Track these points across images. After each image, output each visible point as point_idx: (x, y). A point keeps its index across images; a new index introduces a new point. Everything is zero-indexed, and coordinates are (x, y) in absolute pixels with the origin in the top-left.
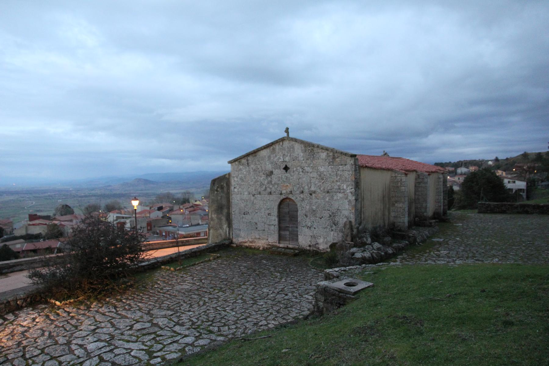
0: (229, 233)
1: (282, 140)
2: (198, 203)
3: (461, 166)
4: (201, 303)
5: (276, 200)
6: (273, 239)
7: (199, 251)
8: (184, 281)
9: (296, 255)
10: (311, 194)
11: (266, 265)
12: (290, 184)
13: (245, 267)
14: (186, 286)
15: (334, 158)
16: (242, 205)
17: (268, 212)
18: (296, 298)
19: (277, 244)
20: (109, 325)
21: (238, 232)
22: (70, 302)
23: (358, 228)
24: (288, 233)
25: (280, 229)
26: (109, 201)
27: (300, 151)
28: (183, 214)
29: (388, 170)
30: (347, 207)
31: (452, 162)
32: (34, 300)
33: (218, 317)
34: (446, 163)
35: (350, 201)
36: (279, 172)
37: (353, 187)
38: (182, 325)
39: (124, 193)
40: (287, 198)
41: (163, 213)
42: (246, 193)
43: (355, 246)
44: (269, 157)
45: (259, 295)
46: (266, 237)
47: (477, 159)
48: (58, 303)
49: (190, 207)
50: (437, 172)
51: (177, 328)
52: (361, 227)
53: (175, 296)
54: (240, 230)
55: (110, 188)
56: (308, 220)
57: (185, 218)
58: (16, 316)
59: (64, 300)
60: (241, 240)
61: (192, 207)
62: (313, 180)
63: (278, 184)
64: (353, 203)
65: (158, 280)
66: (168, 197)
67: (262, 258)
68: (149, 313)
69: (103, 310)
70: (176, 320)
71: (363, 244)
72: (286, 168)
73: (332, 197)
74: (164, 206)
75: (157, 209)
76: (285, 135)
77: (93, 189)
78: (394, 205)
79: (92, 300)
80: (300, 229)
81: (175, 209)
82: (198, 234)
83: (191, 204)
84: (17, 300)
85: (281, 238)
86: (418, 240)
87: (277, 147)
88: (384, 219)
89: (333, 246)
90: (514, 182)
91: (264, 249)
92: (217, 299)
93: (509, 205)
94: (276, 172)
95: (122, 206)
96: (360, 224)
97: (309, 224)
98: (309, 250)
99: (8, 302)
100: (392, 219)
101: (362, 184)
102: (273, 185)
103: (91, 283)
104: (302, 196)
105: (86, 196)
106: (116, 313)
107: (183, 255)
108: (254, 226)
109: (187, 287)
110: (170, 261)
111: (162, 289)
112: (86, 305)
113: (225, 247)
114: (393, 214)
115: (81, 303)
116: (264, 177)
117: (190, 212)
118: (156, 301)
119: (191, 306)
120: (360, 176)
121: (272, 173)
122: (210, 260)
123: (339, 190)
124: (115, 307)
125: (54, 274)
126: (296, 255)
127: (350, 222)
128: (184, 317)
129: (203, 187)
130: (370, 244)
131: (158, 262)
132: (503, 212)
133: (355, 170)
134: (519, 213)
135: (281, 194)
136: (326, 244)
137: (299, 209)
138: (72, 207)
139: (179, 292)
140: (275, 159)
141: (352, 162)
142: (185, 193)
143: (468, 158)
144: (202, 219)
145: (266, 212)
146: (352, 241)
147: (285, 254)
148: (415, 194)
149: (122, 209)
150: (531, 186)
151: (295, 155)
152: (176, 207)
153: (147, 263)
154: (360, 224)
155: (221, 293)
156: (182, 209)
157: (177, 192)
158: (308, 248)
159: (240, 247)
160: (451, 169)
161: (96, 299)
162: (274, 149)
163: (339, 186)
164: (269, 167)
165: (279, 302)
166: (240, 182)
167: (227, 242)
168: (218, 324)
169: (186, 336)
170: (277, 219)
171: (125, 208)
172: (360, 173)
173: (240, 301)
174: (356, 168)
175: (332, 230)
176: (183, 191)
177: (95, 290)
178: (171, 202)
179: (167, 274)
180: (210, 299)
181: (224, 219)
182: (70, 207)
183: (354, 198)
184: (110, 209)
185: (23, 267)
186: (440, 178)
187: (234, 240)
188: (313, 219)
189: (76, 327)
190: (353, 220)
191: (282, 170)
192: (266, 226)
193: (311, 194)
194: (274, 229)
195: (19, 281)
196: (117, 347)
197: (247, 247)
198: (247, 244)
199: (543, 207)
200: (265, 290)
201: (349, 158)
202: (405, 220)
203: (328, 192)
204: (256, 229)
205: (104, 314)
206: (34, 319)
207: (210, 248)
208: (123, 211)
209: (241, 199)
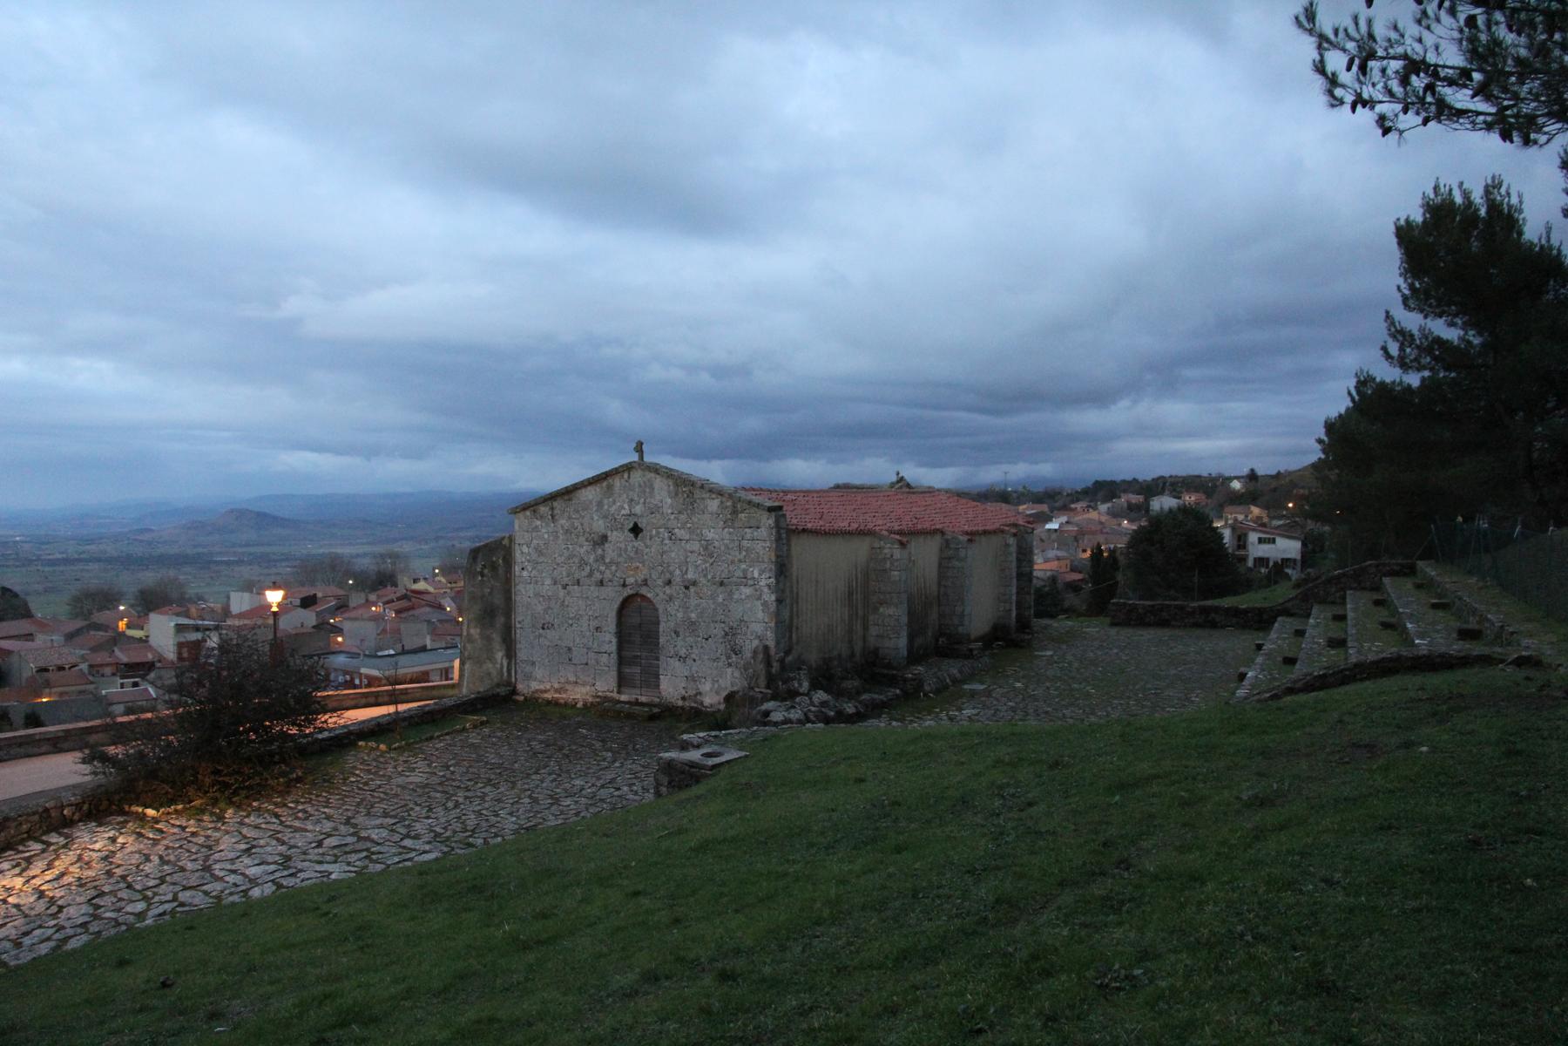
0: (509, 671)
1: (629, 468)
2: (421, 586)
3: (1162, 493)
4: (450, 805)
5: (612, 597)
6: (606, 685)
7: (439, 711)
8: (413, 770)
9: (652, 718)
10: (687, 588)
11: (585, 737)
12: (643, 562)
13: (541, 742)
14: (416, 778)
15: (735, 512)
16: (540, 608)
17: (594, 624)
18: (636, 793)
19: (615, 695)
20: (274, 842)
21: (528, 668)
22: (176, 811)
23: (782, 661)
24: (637, 670)
25: (621, 661)
26: (149, 578)
27: (664, 493)
28: (377, 618)
29: (862, 533)
30: (760, 615)
31: (1141, 478)
32: (98, 807)
33: (484, 824)
34: (1124, 481)
35: (765, 604)
36: (619, 538)
37: (772, 574)
38: (417, 837)
39: (189, 551)
40: (637, 595)
41: (318, 614)
42: (548, 581)
43: (774, 698)
44: (600, 504)
45: (566, 790)
46: (589, 679)
47: (1205, 474)
48: (151, 812)
49: (399, 599)
50: (1003, 531)
51: (408, 843)
52: (790, 658)
53: (396, 795)
54: (533, 663)
55: (147, 537)
56: (680, 643)
57: (384, 631)
58: (70, 840)
59: (162, 806)
60: (535, 686)
61: (404, 597)
62: (692, 558)
63: (617, 564)
64: (773, 608)
65: (355, 768)
66: (335, 568)
67: (580, 725)
68: (348, 822)
69: (252, 820)
70: (403, 831)
71: (793, 694)
72: (636, 530)
73: (731, 593)
74: (320, 595)
75: (298, 602)
76: (635, 457)
77: (91, 541)
78: (876, 610)
79: (222, 805)
80: (662, 663)
81: (352, 605)
82: (424, 677)
83: (401, 591)
84: (62, 807)
85: (623, 682)
86: (927, 688)
87: (617, 482)
88: (850, 641)
89: (729, 698)
90: (1274, 541)
91: (585, 705)
92: (483, 798)
93: (1176, 607)
94: (614, 536)
95: (191, 591)
96: (788, 652)
97: (683, 652)
98: (682, 708)
99: (47, 810)
100: (872, 642)
101: (795, 568)
102: (608, 566)
103: (217, 772)
104: (668, 590)
105: (67, 561)
106: (282, 823)
107: (405, 719)
108: (565, 655)
109: (418, 780)
110: (375, 731)
111: (366, 784)
112: (212, 814)
113: (498, 702)
114: (873, 631)
115: (202, 811)
116: (587, 547)
117: (398, 612)
118: (359, 804)
119: (430, 810)
120: (789, 550)
121: (604, 538)
122: (464, 729)
123: (745, 579)
124: (277, 816)
125: (141, 755)
126: (652, 718)
127: (766, 648)
128: (418, 826)
129: (437, 539)
130: (807, 695)
131: (350, 733)
132: (1164, 624)
133: (778, 539)
134: (1197, 625)
135: (624, 585)
136: (717, 693)
137: (662, 618)
138: (22, 596)
139: (403, 788)
140: (613, 509)
141: (771, 522)
142: (382, 556)
143: (1181, 471)
144: (434, 633)
145: (591, 620)
146: (768, 687)
147: (629, 716)
148: (939, 584)
149: (190, 600)
150: (1314, 551)
151: (655, 501)
152: (356, 599)
153: (326, 734)
154: (788, 652)
155: (488, 789)
156: (375, 604)
157: (360, 552)
158: (680, 703)
159: (532, 702)
160: (1136, 499)
161: (231, 803)
162: (610, 487)
163: (745, 571)
164: (599, 525)
165: (602, 800)
166: (534, 556)
167: (502, 691)
168: (484, 835)
169: (425, 852)
170: (614, 640)
171: (200, 598)
172: (789, 545)
173: (527, 800)
174: (778, 533)
175: (730, 665)
176: (379, 549)
177: (227, 785)
178: (342, 584)
179: (373, 755)
180: (466, 798)
181: (496, 637)
182: (16, 595)
183: (773, 597)
184: (150, 602)
185: (44, 749)
186: (1007, 545)
187: (520, 687)
188: (690, 640)
189: (210, 848)
190: (771, 643)
191: (626, 532)
192: (591, 655)
193: (687, 588)
194: (609, 661)
195: (63, 772)
196: (301, 871)
197: (549, 702)
198: (548, 696)
199: (1246, 611)
200: (577, 782)
201: (765, 515)
202: (899, 644)
203: (722, 584)
204: (568, 665)
205: (257, 827)
206: (113, 840)
207: (464, 703)
208: (193, 610)
209: (537, 595)
